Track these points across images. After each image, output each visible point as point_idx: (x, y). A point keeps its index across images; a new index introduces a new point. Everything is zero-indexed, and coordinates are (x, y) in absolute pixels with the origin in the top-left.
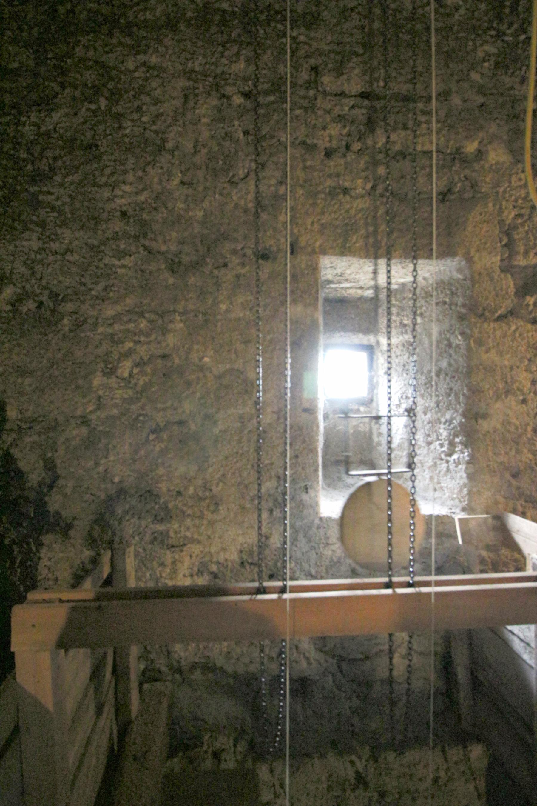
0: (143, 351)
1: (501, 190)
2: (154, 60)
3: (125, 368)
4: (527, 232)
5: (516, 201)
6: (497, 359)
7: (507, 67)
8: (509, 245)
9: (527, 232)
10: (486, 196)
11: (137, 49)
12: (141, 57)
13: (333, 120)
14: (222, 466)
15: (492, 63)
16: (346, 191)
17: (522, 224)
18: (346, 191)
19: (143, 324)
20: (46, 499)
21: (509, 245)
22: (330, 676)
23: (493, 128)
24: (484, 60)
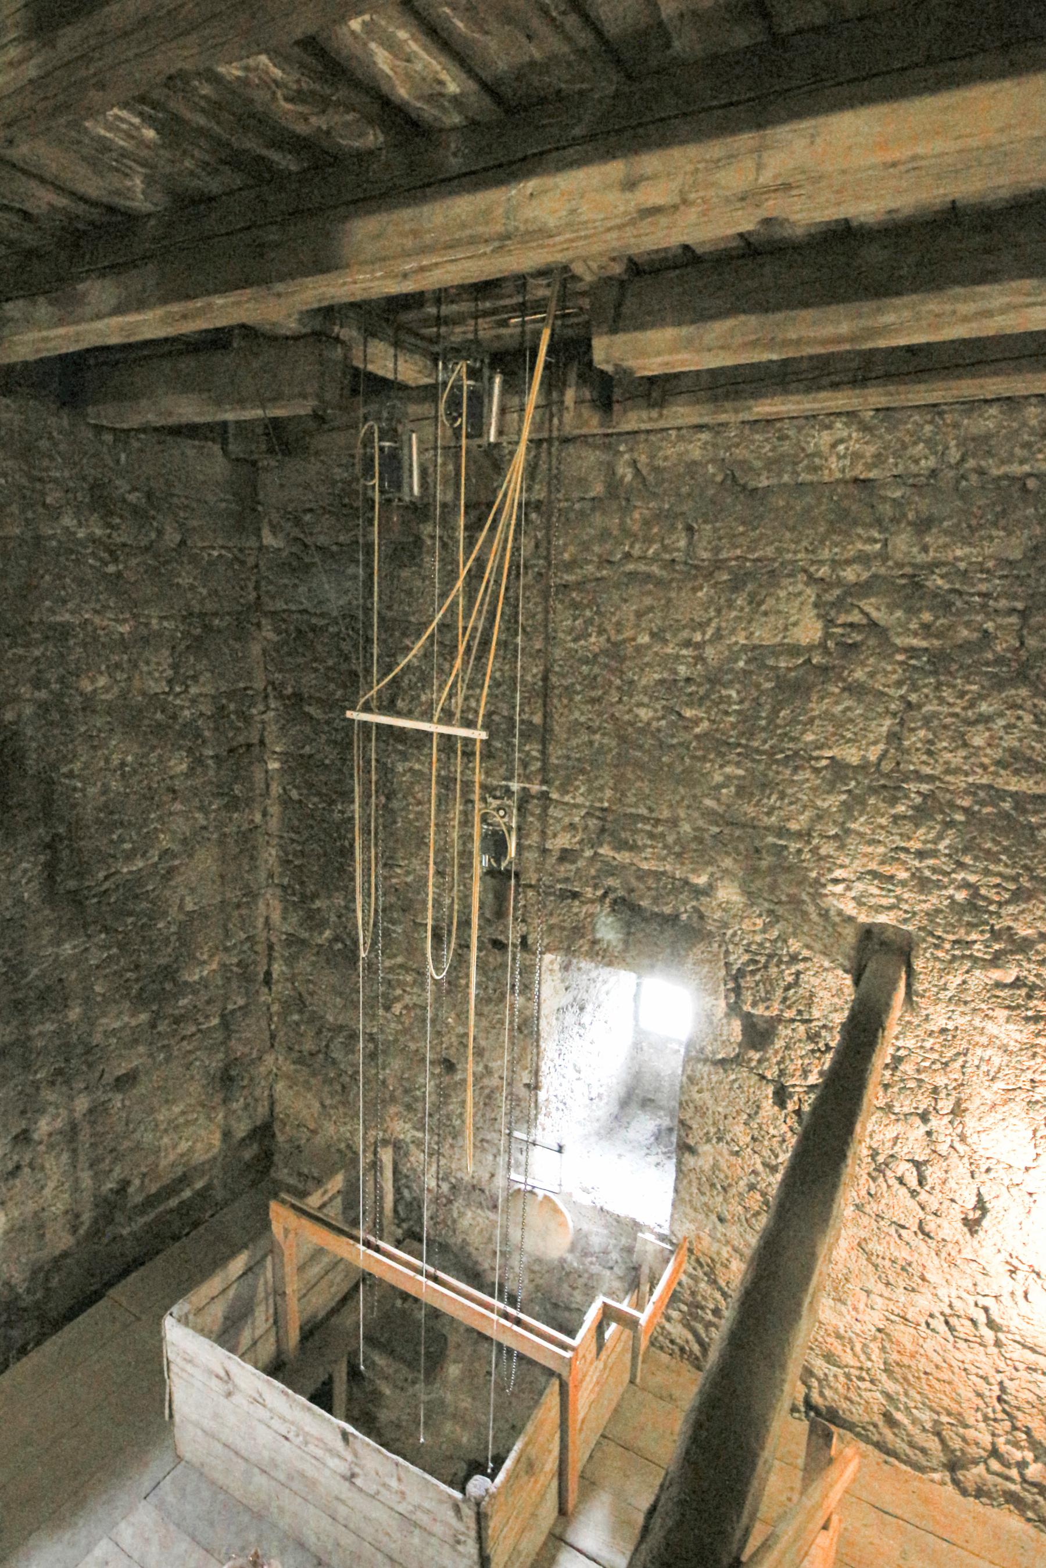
0: (407, 999)
1: (730, 932)
2: (417, 767)
3: (397, 1008)
4: (757, 984)
5: (749, 945)
6: (710, 1103)
7: (752, 794)
8: (737, 990)
9: (757, 984)
10: (710, 934)
11: (404, 757)
12: (408, 765)
13: (564, 829)
14: (924, 1117)
15: (733, 789)
16: (575, 895)
17: (753, 973)
18: (575, 895)
19: (409, 978)
20: (934, 530)
21: (737, 990)
22: (389, 1150)
23: (728, 863)
24: (723, 786)
